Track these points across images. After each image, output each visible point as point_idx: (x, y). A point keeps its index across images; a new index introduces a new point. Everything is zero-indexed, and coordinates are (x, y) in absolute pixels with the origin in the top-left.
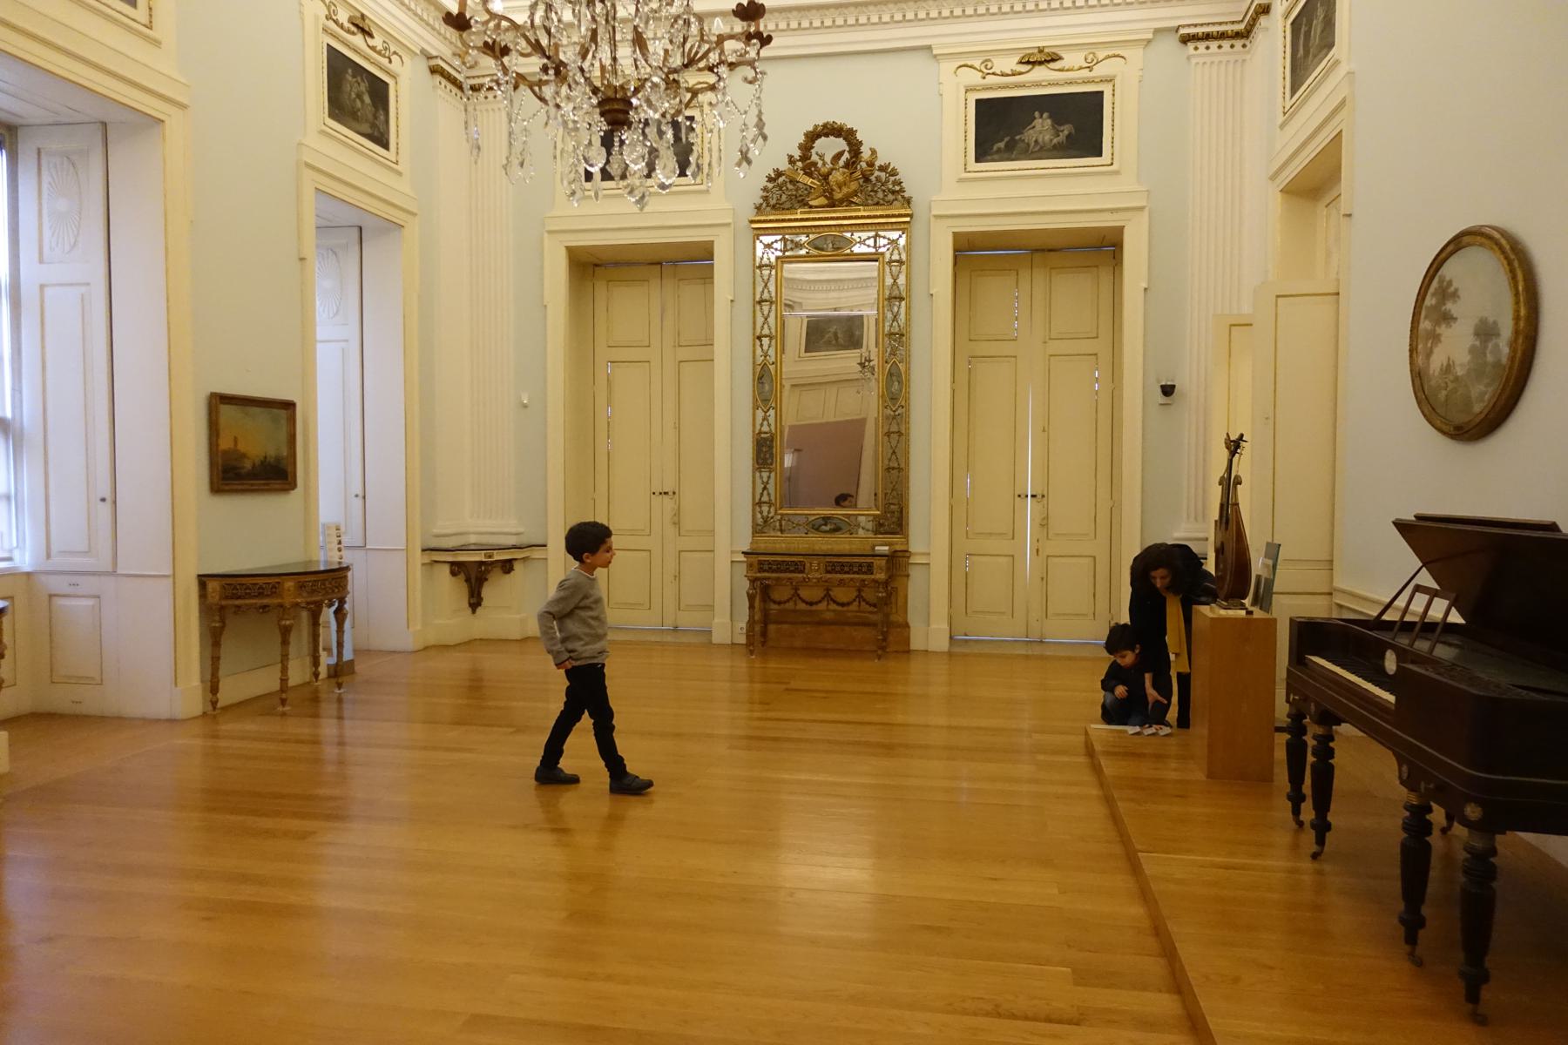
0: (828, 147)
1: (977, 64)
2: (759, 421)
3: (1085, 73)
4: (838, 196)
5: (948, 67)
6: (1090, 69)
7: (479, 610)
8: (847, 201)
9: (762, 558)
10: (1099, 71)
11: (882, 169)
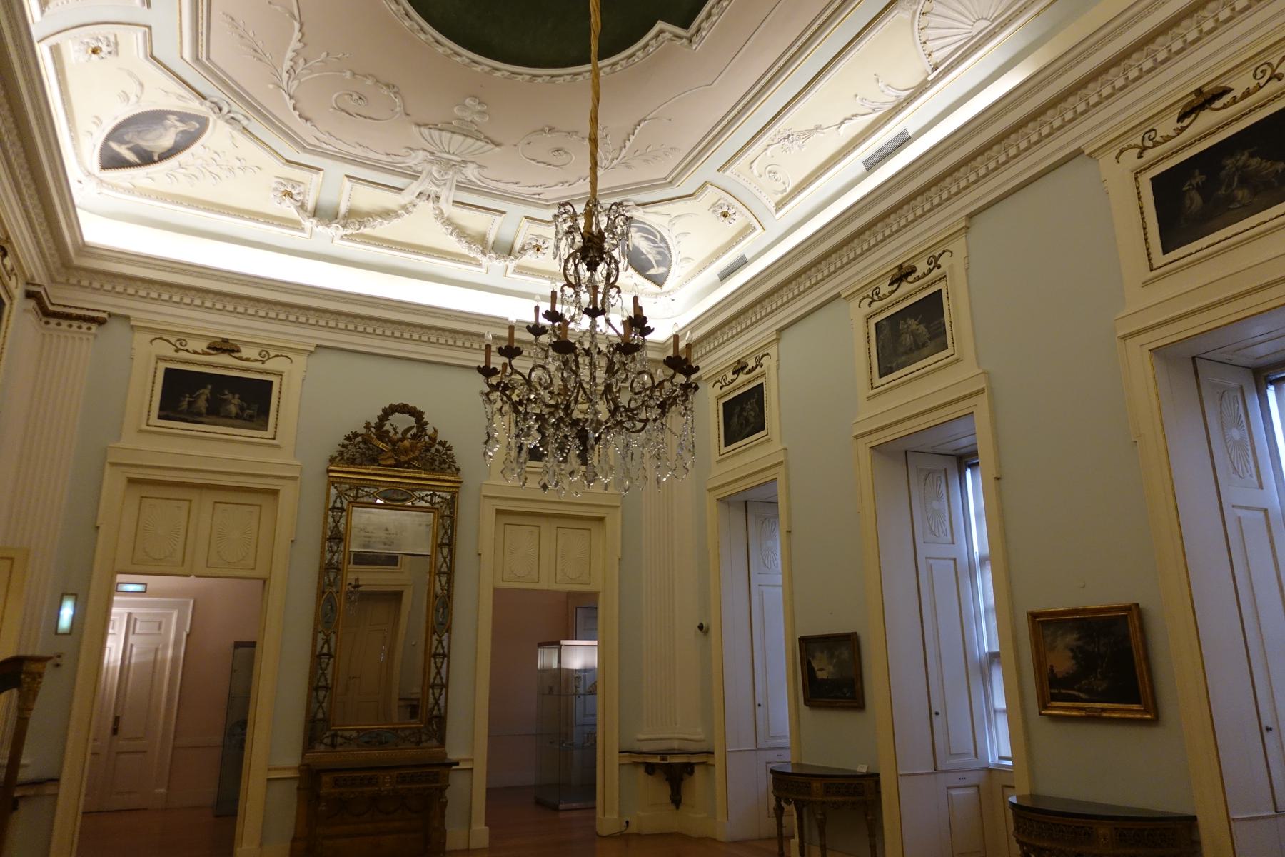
0: (402, 422)
1: (173, 340)
2: (320, 642)
3: (258, 365)
4: (403, 458)
5: (142, 339)
6: (263, 362)
7: (681, 807)
8: (408, 464)
9: (404, 772)
10: (271, 365)
11: (443, 444)
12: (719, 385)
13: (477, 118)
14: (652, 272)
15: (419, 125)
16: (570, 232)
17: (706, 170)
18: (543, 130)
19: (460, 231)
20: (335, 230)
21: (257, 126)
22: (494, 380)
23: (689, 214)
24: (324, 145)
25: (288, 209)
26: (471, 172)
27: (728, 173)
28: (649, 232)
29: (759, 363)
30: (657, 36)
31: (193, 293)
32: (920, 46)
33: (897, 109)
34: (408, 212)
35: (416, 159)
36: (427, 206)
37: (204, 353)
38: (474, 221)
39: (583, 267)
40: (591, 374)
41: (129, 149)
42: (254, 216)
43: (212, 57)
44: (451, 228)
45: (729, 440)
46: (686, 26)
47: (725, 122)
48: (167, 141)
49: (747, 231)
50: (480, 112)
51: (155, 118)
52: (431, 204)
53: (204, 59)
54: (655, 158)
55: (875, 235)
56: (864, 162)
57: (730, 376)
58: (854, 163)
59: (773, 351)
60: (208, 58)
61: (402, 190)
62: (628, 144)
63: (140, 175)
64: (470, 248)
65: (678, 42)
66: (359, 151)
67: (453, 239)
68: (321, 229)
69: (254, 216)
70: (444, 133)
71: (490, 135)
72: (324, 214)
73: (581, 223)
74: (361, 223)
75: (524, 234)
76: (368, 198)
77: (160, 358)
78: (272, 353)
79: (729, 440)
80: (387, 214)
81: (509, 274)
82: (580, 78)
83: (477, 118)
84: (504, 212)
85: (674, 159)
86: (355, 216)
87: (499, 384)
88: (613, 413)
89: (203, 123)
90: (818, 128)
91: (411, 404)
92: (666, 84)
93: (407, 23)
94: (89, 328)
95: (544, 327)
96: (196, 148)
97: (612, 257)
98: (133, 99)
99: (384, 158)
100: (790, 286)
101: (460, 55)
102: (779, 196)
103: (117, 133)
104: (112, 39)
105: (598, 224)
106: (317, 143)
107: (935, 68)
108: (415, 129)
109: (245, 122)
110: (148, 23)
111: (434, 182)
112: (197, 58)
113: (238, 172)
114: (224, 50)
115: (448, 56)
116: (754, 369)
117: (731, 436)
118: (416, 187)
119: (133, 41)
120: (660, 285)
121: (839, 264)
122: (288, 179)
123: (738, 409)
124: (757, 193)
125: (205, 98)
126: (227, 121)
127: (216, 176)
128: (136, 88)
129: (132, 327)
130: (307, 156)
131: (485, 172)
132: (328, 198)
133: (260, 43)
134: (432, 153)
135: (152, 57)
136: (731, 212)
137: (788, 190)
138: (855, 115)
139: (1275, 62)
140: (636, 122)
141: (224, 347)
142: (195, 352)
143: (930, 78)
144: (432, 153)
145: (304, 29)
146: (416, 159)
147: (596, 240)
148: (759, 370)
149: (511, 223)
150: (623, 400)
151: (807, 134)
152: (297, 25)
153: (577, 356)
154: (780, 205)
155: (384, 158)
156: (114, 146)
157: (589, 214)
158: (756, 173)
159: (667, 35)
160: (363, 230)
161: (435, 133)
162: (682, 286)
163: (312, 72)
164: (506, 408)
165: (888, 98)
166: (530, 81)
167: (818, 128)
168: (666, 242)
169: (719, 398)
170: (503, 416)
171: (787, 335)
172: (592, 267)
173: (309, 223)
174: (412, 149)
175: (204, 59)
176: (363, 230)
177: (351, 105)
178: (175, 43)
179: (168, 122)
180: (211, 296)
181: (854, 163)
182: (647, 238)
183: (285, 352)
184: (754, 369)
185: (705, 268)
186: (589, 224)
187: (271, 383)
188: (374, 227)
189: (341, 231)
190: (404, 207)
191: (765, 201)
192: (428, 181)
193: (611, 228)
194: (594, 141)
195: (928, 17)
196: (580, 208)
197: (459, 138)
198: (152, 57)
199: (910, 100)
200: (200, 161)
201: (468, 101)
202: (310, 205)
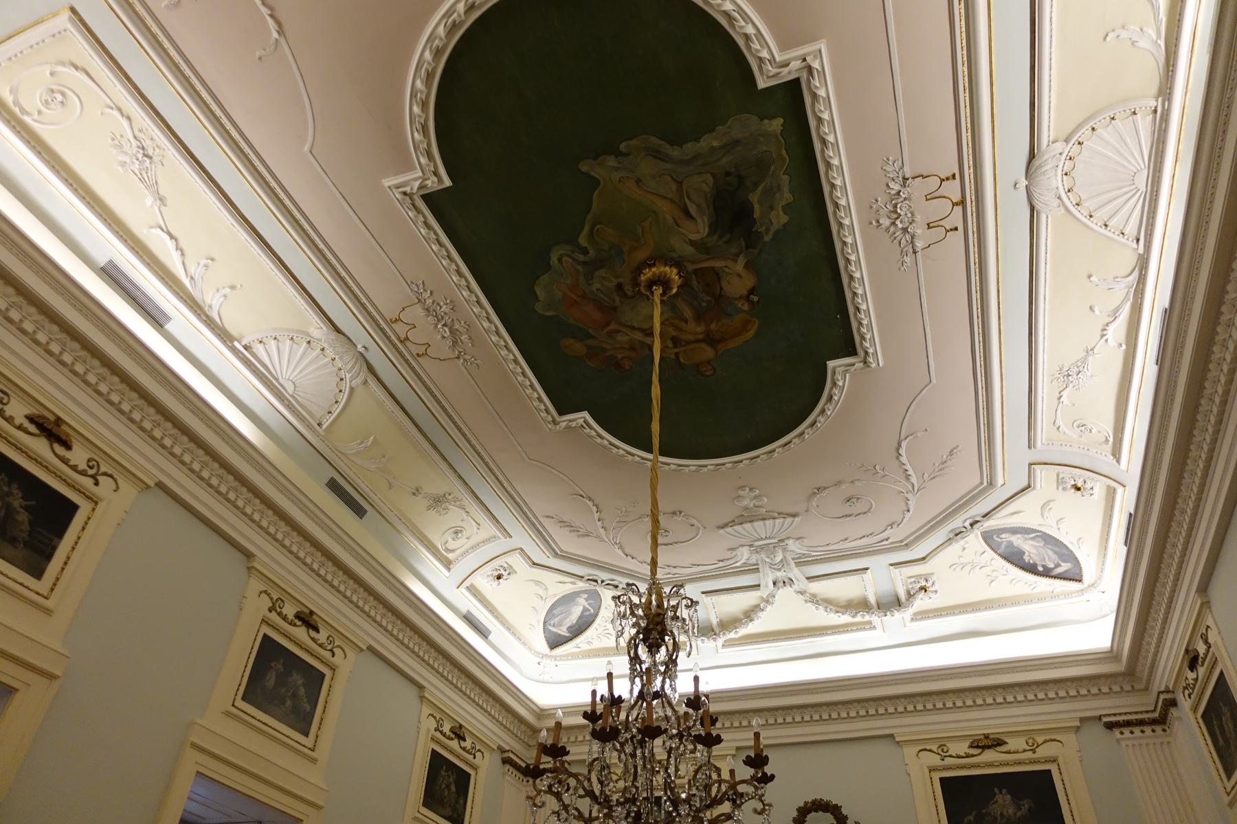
1: (934, 748)
3: (1029, 755)
5: (910, 751)
10: (1042, 752)
31: (1034, 687)
34: (767, 602)
36: (784, 593)
49: (1111, 494)
50: (756, 497)
51: (568, 599)
52: (788, 589)
57: (1191, 675)
67: (832, 615)
70: (767, 522)
77: (932, 770)
107: (246, 347)
139: (103, 469)
142: (959, 757)
143: (236, 344)
154: (1116, 453)
161: (737, 528)
165: (212, 300)
172: (653, 648)
180: (1000, 690)
185: (1106, 548)
199: (209, 322)
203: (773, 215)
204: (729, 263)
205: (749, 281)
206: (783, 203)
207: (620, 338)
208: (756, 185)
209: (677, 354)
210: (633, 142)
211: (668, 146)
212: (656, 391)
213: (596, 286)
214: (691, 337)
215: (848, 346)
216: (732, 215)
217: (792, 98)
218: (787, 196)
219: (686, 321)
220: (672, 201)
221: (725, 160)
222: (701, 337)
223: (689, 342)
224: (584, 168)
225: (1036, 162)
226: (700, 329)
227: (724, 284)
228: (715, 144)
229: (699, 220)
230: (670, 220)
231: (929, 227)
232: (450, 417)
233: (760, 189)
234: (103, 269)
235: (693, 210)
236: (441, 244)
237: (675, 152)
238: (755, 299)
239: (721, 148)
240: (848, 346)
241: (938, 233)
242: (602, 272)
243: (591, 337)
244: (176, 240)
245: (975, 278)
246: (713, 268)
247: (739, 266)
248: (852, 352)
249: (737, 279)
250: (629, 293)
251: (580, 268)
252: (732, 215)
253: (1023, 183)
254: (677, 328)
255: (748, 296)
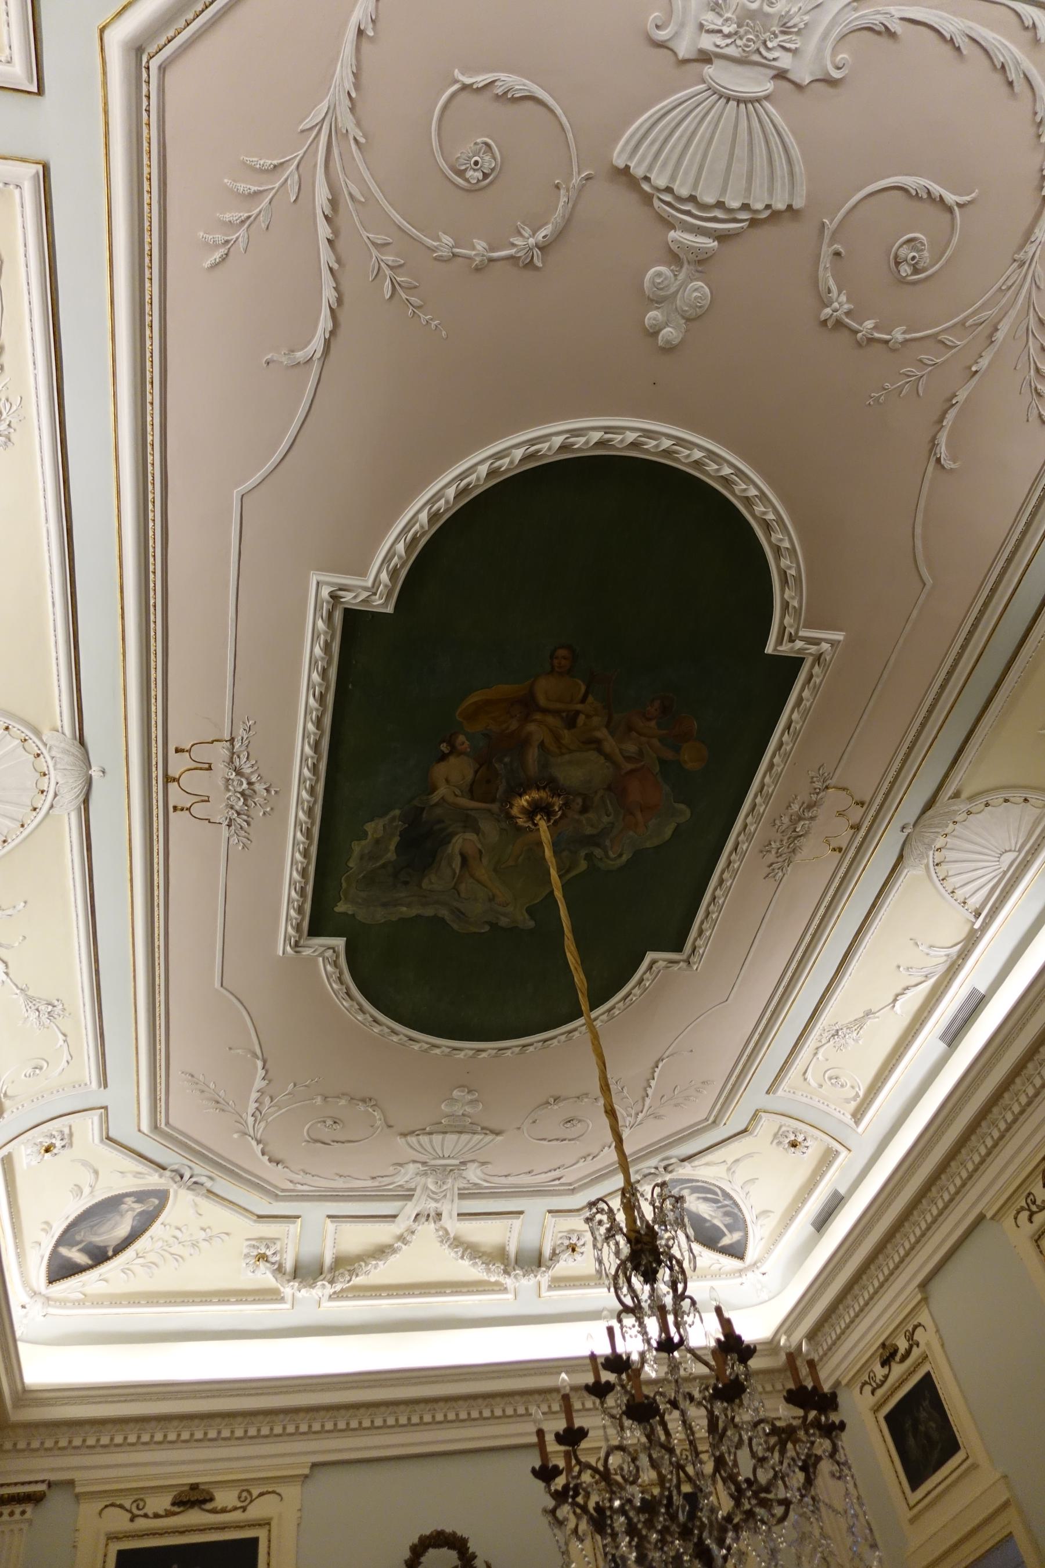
1: (127, 1504)
3: (237, 1516)
5: (89, 1509)
6: (244, 1509)
10: (255, 1512)
12: (868, 1389)
13: (469, 1109)
14: (726, 1241)
15: (404, 1135)
16: (610, 1235)
17: (753, 1096)
18: (548, 1103)
19: (472, 1251)
20: (322, 1290)
21: (224, 1186)
22: (560, 1482)
23: (750, 1155)
24: (299, 1187)
25: (264, 1277)
26: (473, 1174)
27: (780, 1092)
28: (706, 1191)
29: (913, 1344)
30: (650, 968)
32: (948, 897)
33: (953, 969)
35: (407, 1175)
37: (169, 1514)
38: (487, 1233)
39: (637, 1281)
40: (688, 1424)
41: (80, 1250)
42: (224, 1296)
43: (171, 1121)
44: (460, 1250)
45: (916, 1478)
46: (679, 949)
47: (756, 1036)
48: (123, 1230)
49: (828, 1158)
51: (111, 1205)
52: (431, 1226)
53: (163, 1126)
54: (687, 1098)
55: (995, 1124)
56: (942, 1038)
57: (880, 1372)
58: (929, 1041)
59: (924, 1317)
60: (167, 1123)
61: (395, 1216)
62: (650, 1091)
63: (91, 1281)
64: (488, 1270)
65: (676, 967)
66: (340, 1184)
67: (466, 1263)
68: (304, 1293)
69: (224, 1296)
70: (434, 1136)
71: (486, 1124)
72: (305, 1273)
73: (621, 1217)
74: (352, 1273)
75: (552, 1232)
76: (357, 1237)
77: (112, 1537)
78: (255, 1492)
79: (916, 1478)
80: (382, 1252)
81: (545, 1294)
82: (576, 1034)
83: (469, 1109)
84: (521, 1213)
85: (710, 1095)
86: (345, 1264)
87: (566, 1487)
88: (737, 1497)
89: (163, 1196)
90: (868, 1013)
91: (448, 1530)
92: (677, 1016)
93: (377, 1029)
94: (23, 1513)
95: (608, 1383)
96: (156, 1229)
97: (671, 1257)
98: (87, 1190)
99: (369, 1183)
100: (912, 1219)
101: (438, 1047)
102: (853, 1105)
103: (66, 1238)
104: (66, 1131)
105: (642, 1217)
106: (291, 1186)
107: (978, 915)
108: (401, 1141)
109: (209, 1184)
110: (104, 1105)
111: (433, 1197)
112: (155, 1127)
113: (204, 1245)
114: (186, 1112)
115: (426, 1051)
116: (908, 1352)
117: (916, 1471)
118: (411, 1209)
119: (88, 1127)
120: (741, 1257)
121: (964, 1175)
122: (261, 1239)
123: (908, 1424)
124: (824, 1108)
125: (164, 1169)
126: (189, 1188)
127: (178, 1258)
128: (90, 1177)
129: (77, 1497)
130: (282, 1204)
131: (489, 1168)
132: (309, 1251)
133: (222, 1093)
134: (424, 1163)
135: (108, 1138)
136: (800, 1138)
137: (861, 1093)
138: (907, 988)
140: (652, 1064)
141: (193, 1497)
142: (156, 1516)
143: (976, 926)
144: (424, 1163)
145: (267, 1066)
146: (407, 1175)
147: (646, 1239)
148: (916, 1352)
149: (535, 1225)
150: (745, 1467)
151: (859, 1023)
152: (260, 1064)
153: (662, 1417)
154: (858, 1115)
155: (369, 1183)
156: (64, 1251)
157: (630, 1206)
158: (812, 1082)
159: (661, 964)
160: (357, 1281)
161: (424, 1139)
162: (769, 1251)
163: (280, 1109)
164: (584, 1526)
165: (938, 961)
166: (521, 1053)
167: (868, 1013)
168: (731, 1198)
169: (876, 1410)
170: (582, 1541)
171: (937, 1288)
172: (650, 1277)
173: (288, 1290)
174: (401, 1165)
175: (163, 1126)
176: (357, 1281)
177: (325, 1133)
178: (132, 1119)
179: (124, 1207)
181: (929, 1041)
182: (706, 1199)
183: (271, 1485)
184: (908, 1352)
186: (631, 1220)
187: (255, 1541)
188: (367, 1273)
189: (329, 1290)
190: (401, 1238)
191: (836, 1114)
192: (424, 1197)
193: (661, 1217)
194: (611, 1113)
195: (944, 867)
196: (616, 1203)
197: (451, 1138)
198: (108, 1138)
199: (964, 954)
200: (160, 1243)
201: (456, 1093)
202: (289, 1266)
203: (380, 833)
204: (451, 799)
205: (440, 771)
206: (363, 842)
207: (631, 748)
208: (384, 866)
209: (583, 701)
210: (476, 930)
211: (447, 918)
212: (572, 957)
213: (605, 819)
214: (550, 719)
215: (355, 627)
216: (421, 844)
217: (319, 921)
218: (357, 847)
219: (542, 745)
220: (472, 876)
221: (402, 895)
222: (538, 716)
223: (556, 713)
224: (531, 924)
225: (81, 798)
226: (532, 727)
227: (470, 777)
228: (404, 909)
229: (457, 851)
230: (485, 861)
231: (210, 764)
232: (943, 687)
233: (382, 862)
234: (949, 1045)
235: (457, 863)
236: (708, 913)
237: (444, 913)
238: (444, 747)
239: (402, 905)
240: (355, 627)
241: (202, 754)
242: (589, 831)
243: (662, 762)
244: (897, 995)
245: (157, 675)
246: (472, 799)
247: (442, 791)
248: (350, 614)
249: (452, 776)
250: (579, 800)
251: (608, 843)
252: (421, 844)
253: (95, 772)
254: (557, 738)
255: (451, 753)
